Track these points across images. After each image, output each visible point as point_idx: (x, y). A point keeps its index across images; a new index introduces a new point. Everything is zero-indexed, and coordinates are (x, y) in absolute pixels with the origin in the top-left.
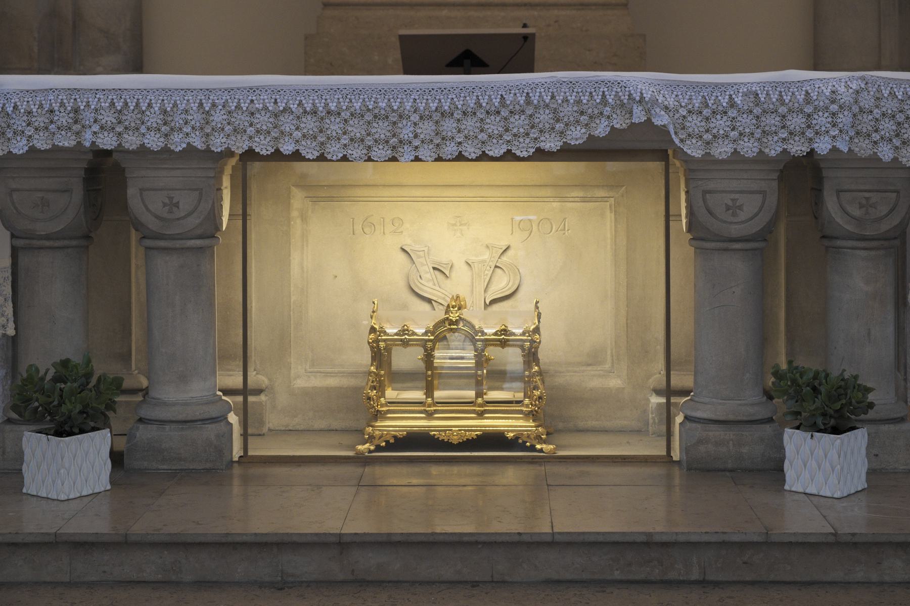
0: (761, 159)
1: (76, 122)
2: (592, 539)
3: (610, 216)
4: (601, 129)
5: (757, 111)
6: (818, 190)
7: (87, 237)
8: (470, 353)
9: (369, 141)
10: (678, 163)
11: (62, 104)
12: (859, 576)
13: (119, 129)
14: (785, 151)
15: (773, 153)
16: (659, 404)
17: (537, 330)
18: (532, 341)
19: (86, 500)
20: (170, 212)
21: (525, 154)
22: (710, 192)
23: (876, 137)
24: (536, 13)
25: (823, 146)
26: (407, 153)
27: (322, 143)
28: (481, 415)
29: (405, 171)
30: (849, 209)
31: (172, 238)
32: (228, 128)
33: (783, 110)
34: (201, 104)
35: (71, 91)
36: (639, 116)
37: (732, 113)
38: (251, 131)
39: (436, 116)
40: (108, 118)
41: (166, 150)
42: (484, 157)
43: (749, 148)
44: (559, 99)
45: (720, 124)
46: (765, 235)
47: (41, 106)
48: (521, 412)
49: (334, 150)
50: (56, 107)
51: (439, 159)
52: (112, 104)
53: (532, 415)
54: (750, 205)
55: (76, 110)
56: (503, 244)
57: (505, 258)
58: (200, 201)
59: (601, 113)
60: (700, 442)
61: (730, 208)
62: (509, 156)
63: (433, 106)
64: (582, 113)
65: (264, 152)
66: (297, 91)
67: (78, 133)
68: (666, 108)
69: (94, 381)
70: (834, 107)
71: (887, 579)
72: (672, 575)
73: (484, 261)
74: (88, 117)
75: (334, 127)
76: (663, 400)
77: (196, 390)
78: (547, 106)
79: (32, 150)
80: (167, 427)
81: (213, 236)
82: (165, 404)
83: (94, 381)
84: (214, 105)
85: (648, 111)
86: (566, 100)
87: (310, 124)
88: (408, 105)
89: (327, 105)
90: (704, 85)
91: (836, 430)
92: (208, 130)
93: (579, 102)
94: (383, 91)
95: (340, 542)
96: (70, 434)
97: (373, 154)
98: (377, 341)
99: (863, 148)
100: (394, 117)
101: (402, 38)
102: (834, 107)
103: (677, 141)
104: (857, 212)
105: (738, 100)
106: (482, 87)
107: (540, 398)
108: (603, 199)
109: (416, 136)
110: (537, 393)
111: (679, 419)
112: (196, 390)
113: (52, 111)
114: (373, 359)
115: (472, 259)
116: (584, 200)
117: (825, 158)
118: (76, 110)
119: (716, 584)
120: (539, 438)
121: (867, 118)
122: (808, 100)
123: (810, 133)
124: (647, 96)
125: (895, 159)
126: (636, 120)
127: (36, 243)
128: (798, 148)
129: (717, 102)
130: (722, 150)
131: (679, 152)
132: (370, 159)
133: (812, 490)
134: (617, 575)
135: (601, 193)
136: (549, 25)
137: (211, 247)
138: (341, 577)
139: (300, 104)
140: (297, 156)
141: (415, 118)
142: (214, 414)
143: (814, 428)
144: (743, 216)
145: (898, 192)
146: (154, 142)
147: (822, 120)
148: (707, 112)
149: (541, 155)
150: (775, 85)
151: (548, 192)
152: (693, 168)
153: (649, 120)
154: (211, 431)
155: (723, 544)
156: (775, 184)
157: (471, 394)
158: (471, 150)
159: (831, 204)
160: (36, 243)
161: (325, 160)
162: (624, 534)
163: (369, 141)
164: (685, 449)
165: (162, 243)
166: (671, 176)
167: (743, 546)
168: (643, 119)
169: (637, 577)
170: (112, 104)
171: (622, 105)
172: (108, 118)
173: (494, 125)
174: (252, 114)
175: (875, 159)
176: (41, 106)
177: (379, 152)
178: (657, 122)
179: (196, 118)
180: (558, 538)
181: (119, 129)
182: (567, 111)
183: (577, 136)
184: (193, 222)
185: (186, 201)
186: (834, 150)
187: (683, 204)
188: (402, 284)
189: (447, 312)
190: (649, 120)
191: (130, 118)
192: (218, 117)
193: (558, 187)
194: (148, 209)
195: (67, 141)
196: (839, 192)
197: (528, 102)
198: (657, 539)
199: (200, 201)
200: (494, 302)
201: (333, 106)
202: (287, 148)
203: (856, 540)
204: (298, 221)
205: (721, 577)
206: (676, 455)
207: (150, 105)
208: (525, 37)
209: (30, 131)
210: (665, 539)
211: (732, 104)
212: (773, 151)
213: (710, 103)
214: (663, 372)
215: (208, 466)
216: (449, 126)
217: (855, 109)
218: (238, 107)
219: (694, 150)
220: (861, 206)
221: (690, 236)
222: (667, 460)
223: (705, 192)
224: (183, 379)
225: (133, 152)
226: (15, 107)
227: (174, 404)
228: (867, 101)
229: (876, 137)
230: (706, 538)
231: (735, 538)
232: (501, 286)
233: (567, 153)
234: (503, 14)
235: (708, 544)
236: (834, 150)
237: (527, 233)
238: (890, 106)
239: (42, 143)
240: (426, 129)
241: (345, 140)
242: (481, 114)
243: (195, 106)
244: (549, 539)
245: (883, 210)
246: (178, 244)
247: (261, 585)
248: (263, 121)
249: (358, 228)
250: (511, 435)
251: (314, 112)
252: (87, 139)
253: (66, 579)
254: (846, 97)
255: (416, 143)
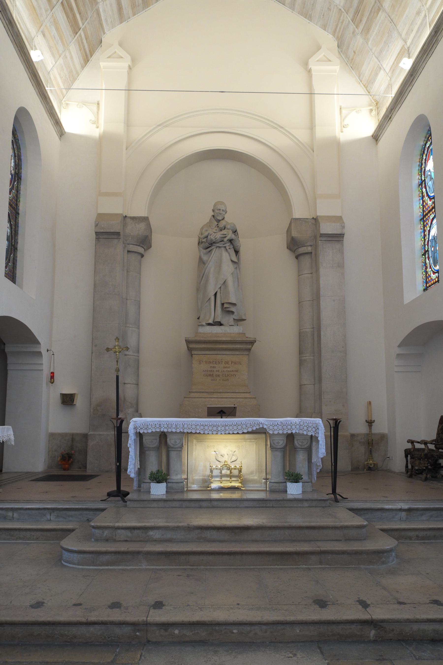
0: (283, 434)
1: (160, 427)
2: (253, 499)
3: (255, 445)
4: (254, 429)
5: (282, 425)
6: (294, 440)
7: (158, 448)
8: (229, 471)
9: (213, 430)
10: (268, 435)
11: (158, 423)
12: (299, 505)
13: (168, 428)
14: (287, 432)
15: (285, 433)
16: (264, 482)
17: (241, 466)
18: (241, 468)
19: (162, 495)
20: (175, 443)
21: (241, 433)
22: (274, 440)
23: (303, 430)
24: (234, 400)
25: (294, 432)
26: (219, 433)
27: (204, 431)
28: (231, 482)
29: (219, 436)
30: (299, 443)
31: (175, 448)
32: (187, 428)
33: (287, 425)
34: (182, 424)
35: (159, 421)
36: (261, 426)
37: (278, 426)
38: (191, 428)
39: (225, 426)
40: (166, 426)
41: (176, 432)
42: (233, 433)
43: (281, 432)
44: (247, 423)
45: (275, 428)
46: (285, 448)
47: (154, 424)
48: (238, 482)
49: (206, 432)
50: (156, 424)
51: (225, 434)
52: (167, 423)
53: (241, 483)
54: (281, 442)
55: (160, 425)
56: (234, 450)
57: (234, 453)
58: (181, 441)
59: (254, 426)
60: (272, 486)
61: (278, 443)
62: (238, 433)
63: (224, 424)
64: (251, 426)
65: (194, 432)
66: (200, 421)
67: (160, 429)
68: (266, 425)
69: (163, 474)
70: (296, 425)
71: (304, 506)
72: (267, 506)
73: (230, 454)
74: (162, 426)
75: (206, 428)
76: (265, 481)
77: (179, 477)
78: (245, 424)
79: (152, 432)
80: (174, 484)
81: (182, 448)
82: (173, 479)
83: (163, 474)
84: (185, 424)
85: (263, 425)
86: (248, 423)
87: (202, 427)
88: (220, 424)
89: (205, 424)
90: (273, 421)
91: (296, 482)
92: (184, 428)
93: (250, 424)
94: (215, 421)
95: (314, 384)
96: (160, 483)
97: (213, 433)
98: (211, 468)
99: (301, 432)
100: (217, 426)
101: (208, 407)
102: (296, 425)
103: (268, 431)
104: (300, 444)
105: (279, 423)
106: (233, 421)
107: (242, 479)
108: (253, 442)
109: (221, 430)
110: (242, 478)
111: (268, 483)
112: (179, 477)
113: (156, 425)
114: (211, 472)
115: (228, 453)
116: (250, 442)
117: (295, 434)
118: (160, 425)
119: (275, 507)
120: (242, 487)
121: (302, 427)
122: (291, 423)
123: (291, 429)
124: (263, 423)
125: (307, 434)
126: (260, 427)
127: (150, 449)
128: (289, 432)
129: (275, 423)
130: (276, 432)
131: (268, 433)
132: (213, 434)
133: (292, 493)
134: (258, 506)
135: (253, 441)
136: (237, 403)
137: (182, 450)
138: (210, 506)
139: (200, 424)
140: (199, 433)
141: (221, 426)
142: (182, 481)
143: (292, 482)
144: (280, 444)
145: (308, 440)
146: (174, 430)
147: (293, 427)
148: (273, 425)
149: (243, 433)
150: (285, 421)
151: (243, 440)
152: (271, 436)
153: (263, 427)
154: (182, 484)
155: (276, 500)
156: (286, 439)
157: (229, 479)
158: (231, 432)
159: (296, 442)
160: (150, 449)
161: (205, 434)
162: (259, 498)
163: (213, 430)
164: (269, 488)
165: (173, 449)
166: (267, 437)
167: (279, 500)
168: (262, 427)
169: (261, 506)
170: (167, 423)
171: (258, 424)
172: (166, 426)
173: (235, 428)
174: (192, 425)
175: (303, 434)
176: (154, 424)
177: (215, 432)
178: (265, 427)
179: (181, 426)
180: (248, 499)
181: (168, 428)
182: (248, 425)
183: (250, 430)
184: (179, 445)
185: (178, 441)
186: (296, 432)
187: (269, 442)
188: (214, 458)
189: (225, 463)
190: (263, 427)
191: (170, 426)
192: (186, 426)
193: (245, 439)
194: (171, 442)
195: (158, 430)
196: (297, 440)
197: (241, 424)
198: (265, 499)
199: (181, 441)
200: (232, 462)
201: (206, 424)
202: (198, 432)
203: (299, 499)
204: (195, 446)
205: (275, 506)
206: (268, 489)
207: (173, 424)
208: (235, 407)
209: (152, 428)
210: (266, 499)
211: (278, 424)
212: (285, 432)
213: (274, 424)
214: (265, 475)
215: (181, 491)
216: (227, 428)
217: (300, 425)
218: (189, 424)
219: (271, 432)
220: (301, 443)
221: (270, 448)
222: (266, 490)
223: (273, 440)
224: (177, 475)
225: (170, 432)
226: (149, 424)
227: (175, 479)
228: (302, 423)
229: (303, 430)
230: (273, 499)
231: (278, 499)
232: (234, 458)
233: (248, 433)
234: (226, 400)
235: (273, 500)
236: (296, 432)
237: (239, 449)
238: (306, 424)
239: (154, 431)
240: (223, 428)
241: (208, 430)
242: (233, 426)
243: (181, 424)
244: (246, 499)
245: (305, 443)
246: (177, 449)
247: (197, 507)
248: (194, 427)
249: (206, 448)
250: (236, 486)
251: (203, 425)
252: (162, 430)
253: (163, 506)
254: (298, 423)
255: (221, 431)
